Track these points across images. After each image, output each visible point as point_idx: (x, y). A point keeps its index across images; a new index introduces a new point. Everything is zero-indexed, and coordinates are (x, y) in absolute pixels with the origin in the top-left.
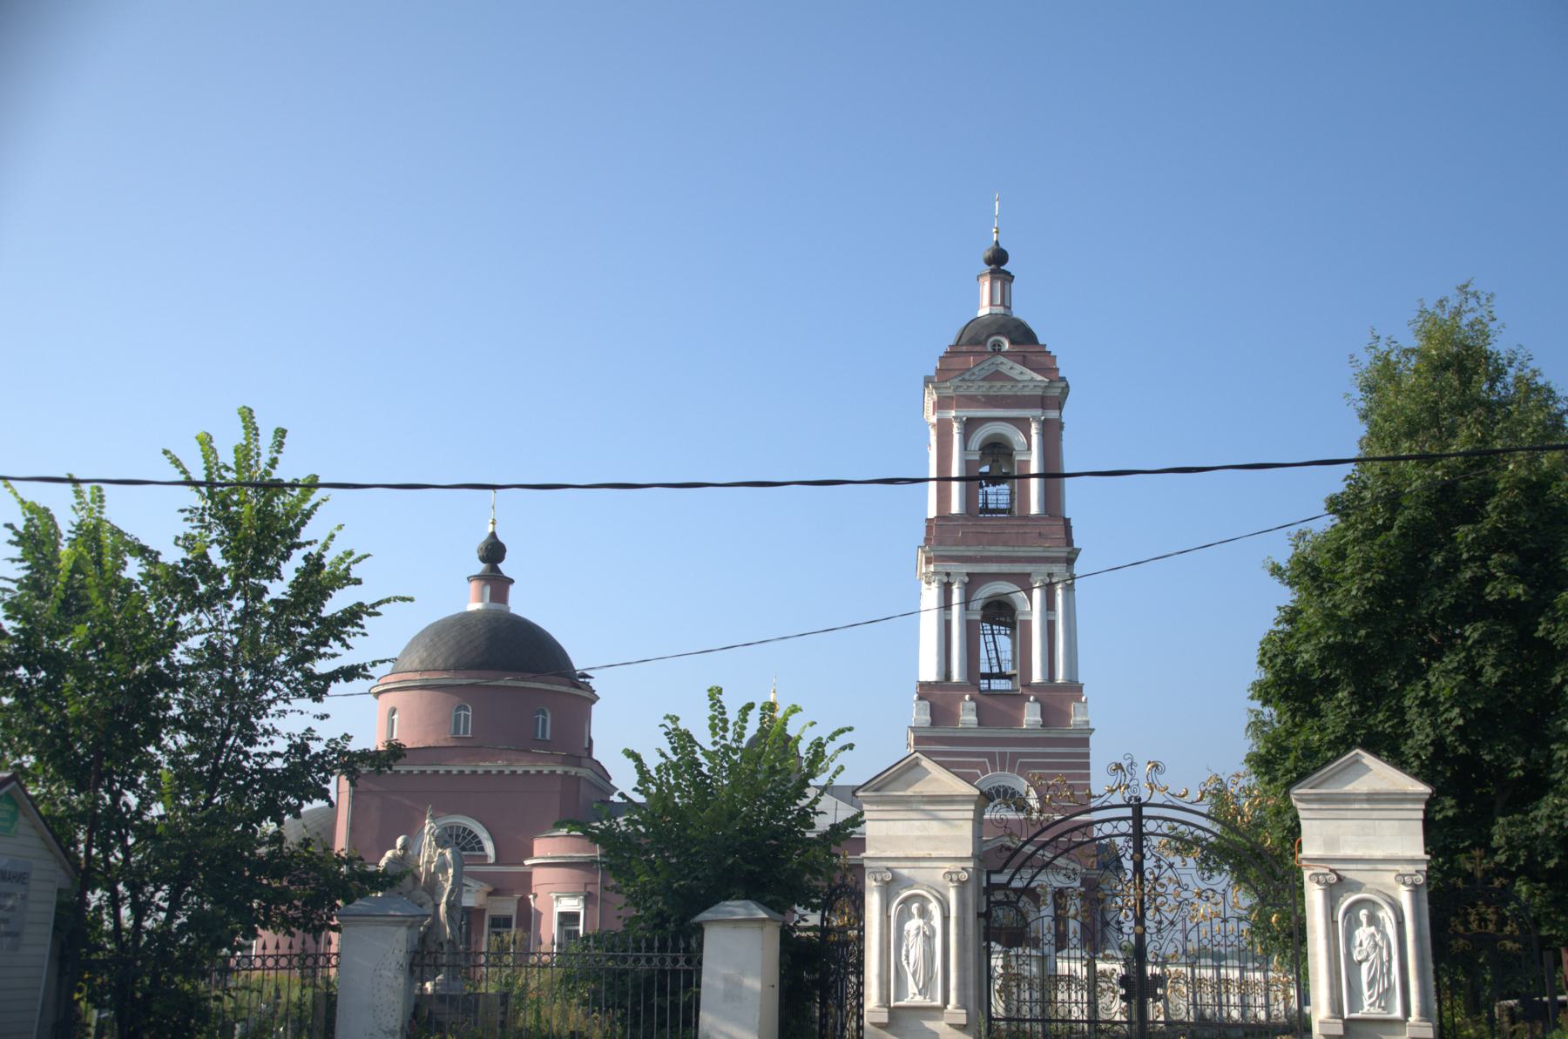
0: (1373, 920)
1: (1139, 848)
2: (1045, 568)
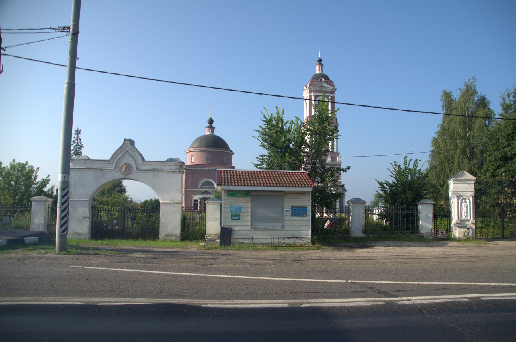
0: (465, 202)
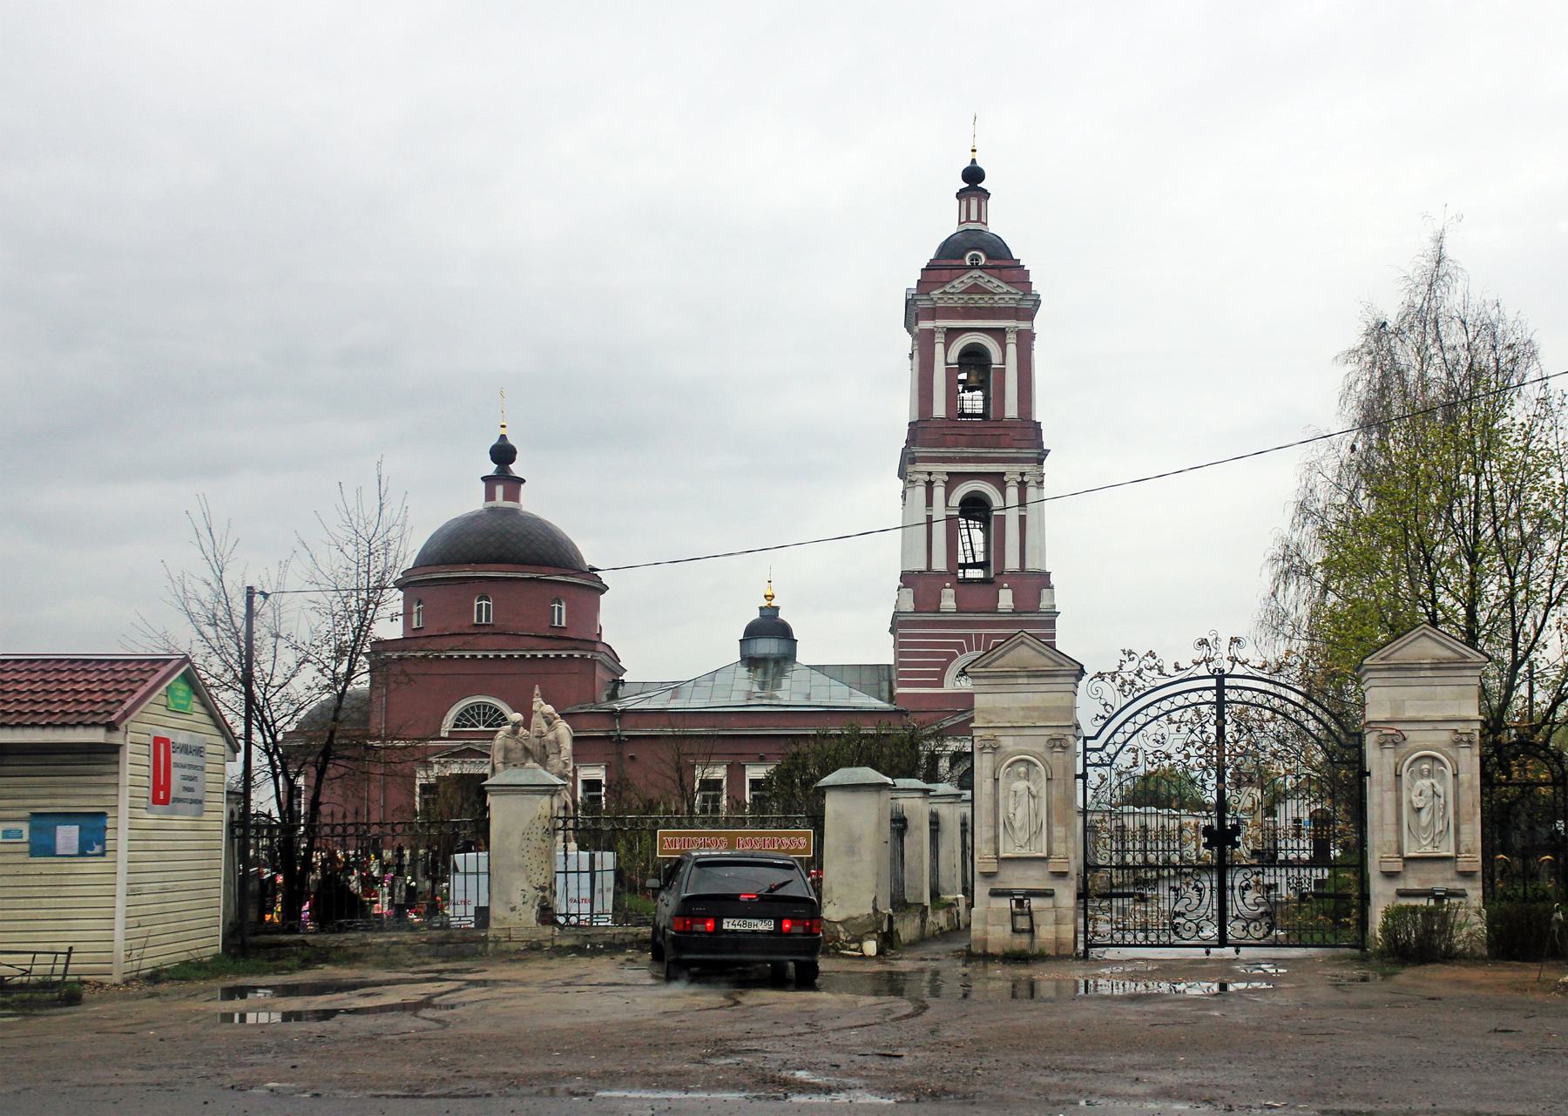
1: (1220, 715)
2: (1017, 468)
